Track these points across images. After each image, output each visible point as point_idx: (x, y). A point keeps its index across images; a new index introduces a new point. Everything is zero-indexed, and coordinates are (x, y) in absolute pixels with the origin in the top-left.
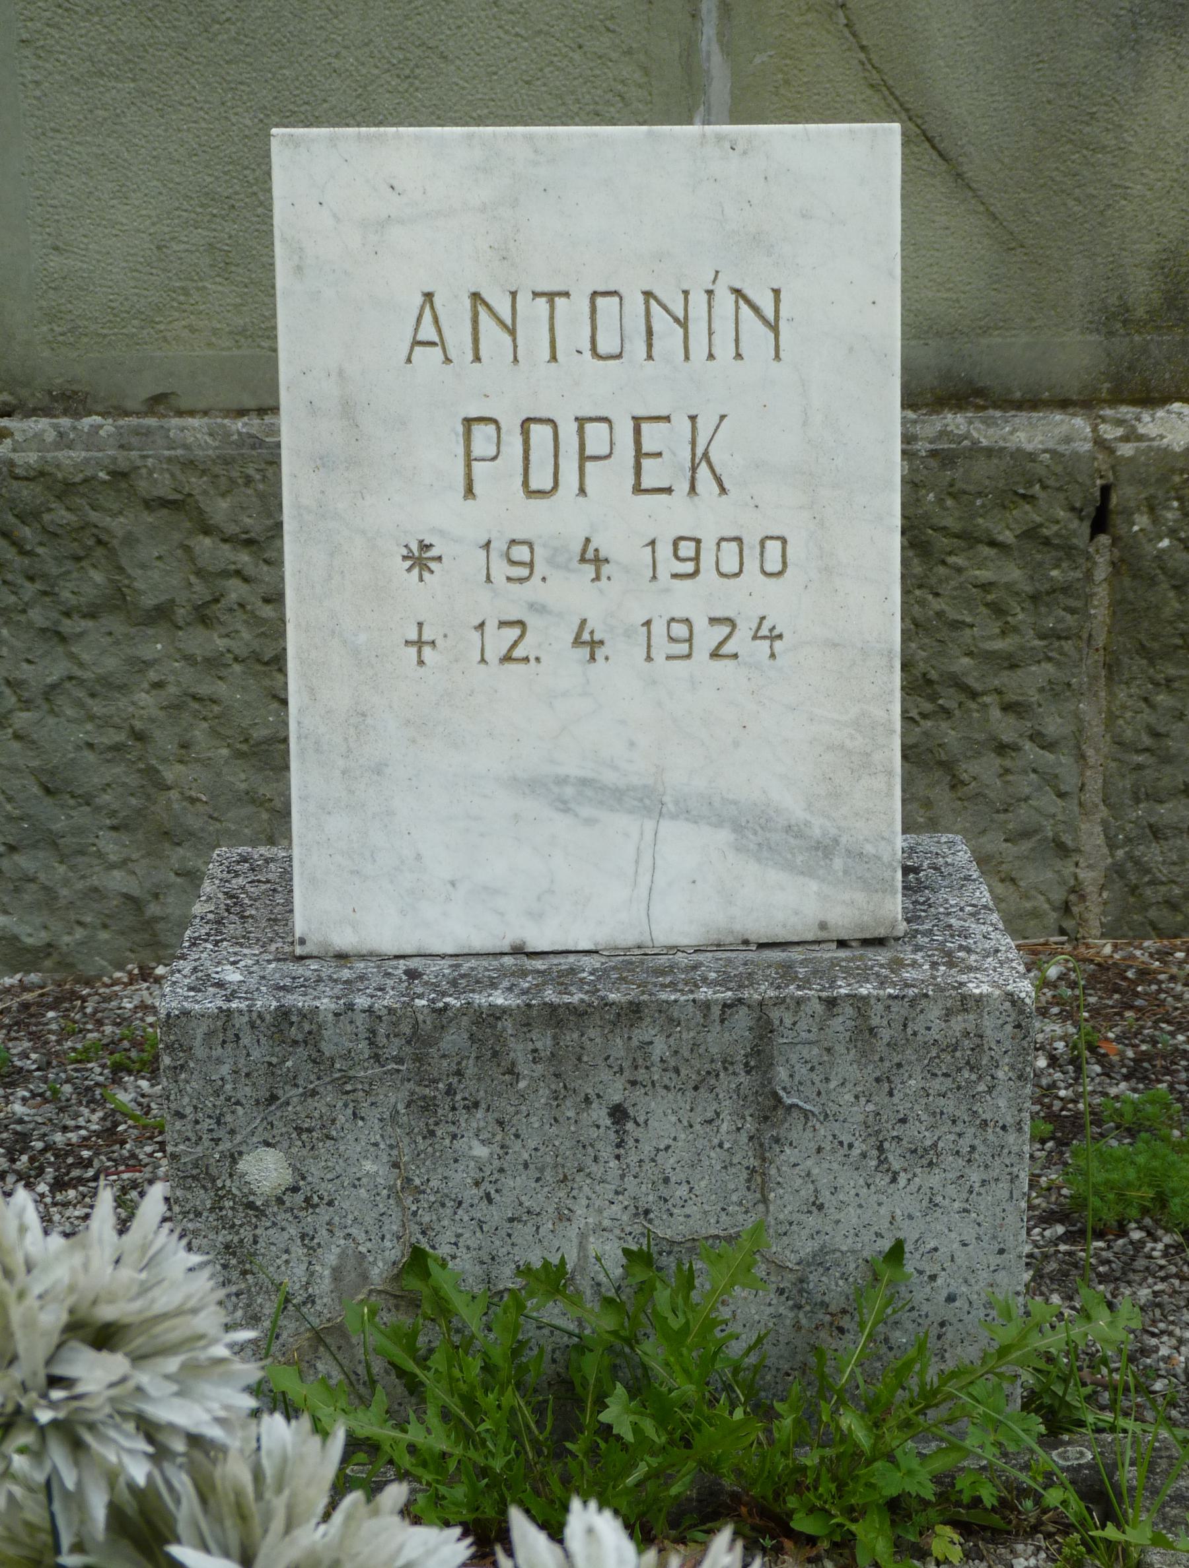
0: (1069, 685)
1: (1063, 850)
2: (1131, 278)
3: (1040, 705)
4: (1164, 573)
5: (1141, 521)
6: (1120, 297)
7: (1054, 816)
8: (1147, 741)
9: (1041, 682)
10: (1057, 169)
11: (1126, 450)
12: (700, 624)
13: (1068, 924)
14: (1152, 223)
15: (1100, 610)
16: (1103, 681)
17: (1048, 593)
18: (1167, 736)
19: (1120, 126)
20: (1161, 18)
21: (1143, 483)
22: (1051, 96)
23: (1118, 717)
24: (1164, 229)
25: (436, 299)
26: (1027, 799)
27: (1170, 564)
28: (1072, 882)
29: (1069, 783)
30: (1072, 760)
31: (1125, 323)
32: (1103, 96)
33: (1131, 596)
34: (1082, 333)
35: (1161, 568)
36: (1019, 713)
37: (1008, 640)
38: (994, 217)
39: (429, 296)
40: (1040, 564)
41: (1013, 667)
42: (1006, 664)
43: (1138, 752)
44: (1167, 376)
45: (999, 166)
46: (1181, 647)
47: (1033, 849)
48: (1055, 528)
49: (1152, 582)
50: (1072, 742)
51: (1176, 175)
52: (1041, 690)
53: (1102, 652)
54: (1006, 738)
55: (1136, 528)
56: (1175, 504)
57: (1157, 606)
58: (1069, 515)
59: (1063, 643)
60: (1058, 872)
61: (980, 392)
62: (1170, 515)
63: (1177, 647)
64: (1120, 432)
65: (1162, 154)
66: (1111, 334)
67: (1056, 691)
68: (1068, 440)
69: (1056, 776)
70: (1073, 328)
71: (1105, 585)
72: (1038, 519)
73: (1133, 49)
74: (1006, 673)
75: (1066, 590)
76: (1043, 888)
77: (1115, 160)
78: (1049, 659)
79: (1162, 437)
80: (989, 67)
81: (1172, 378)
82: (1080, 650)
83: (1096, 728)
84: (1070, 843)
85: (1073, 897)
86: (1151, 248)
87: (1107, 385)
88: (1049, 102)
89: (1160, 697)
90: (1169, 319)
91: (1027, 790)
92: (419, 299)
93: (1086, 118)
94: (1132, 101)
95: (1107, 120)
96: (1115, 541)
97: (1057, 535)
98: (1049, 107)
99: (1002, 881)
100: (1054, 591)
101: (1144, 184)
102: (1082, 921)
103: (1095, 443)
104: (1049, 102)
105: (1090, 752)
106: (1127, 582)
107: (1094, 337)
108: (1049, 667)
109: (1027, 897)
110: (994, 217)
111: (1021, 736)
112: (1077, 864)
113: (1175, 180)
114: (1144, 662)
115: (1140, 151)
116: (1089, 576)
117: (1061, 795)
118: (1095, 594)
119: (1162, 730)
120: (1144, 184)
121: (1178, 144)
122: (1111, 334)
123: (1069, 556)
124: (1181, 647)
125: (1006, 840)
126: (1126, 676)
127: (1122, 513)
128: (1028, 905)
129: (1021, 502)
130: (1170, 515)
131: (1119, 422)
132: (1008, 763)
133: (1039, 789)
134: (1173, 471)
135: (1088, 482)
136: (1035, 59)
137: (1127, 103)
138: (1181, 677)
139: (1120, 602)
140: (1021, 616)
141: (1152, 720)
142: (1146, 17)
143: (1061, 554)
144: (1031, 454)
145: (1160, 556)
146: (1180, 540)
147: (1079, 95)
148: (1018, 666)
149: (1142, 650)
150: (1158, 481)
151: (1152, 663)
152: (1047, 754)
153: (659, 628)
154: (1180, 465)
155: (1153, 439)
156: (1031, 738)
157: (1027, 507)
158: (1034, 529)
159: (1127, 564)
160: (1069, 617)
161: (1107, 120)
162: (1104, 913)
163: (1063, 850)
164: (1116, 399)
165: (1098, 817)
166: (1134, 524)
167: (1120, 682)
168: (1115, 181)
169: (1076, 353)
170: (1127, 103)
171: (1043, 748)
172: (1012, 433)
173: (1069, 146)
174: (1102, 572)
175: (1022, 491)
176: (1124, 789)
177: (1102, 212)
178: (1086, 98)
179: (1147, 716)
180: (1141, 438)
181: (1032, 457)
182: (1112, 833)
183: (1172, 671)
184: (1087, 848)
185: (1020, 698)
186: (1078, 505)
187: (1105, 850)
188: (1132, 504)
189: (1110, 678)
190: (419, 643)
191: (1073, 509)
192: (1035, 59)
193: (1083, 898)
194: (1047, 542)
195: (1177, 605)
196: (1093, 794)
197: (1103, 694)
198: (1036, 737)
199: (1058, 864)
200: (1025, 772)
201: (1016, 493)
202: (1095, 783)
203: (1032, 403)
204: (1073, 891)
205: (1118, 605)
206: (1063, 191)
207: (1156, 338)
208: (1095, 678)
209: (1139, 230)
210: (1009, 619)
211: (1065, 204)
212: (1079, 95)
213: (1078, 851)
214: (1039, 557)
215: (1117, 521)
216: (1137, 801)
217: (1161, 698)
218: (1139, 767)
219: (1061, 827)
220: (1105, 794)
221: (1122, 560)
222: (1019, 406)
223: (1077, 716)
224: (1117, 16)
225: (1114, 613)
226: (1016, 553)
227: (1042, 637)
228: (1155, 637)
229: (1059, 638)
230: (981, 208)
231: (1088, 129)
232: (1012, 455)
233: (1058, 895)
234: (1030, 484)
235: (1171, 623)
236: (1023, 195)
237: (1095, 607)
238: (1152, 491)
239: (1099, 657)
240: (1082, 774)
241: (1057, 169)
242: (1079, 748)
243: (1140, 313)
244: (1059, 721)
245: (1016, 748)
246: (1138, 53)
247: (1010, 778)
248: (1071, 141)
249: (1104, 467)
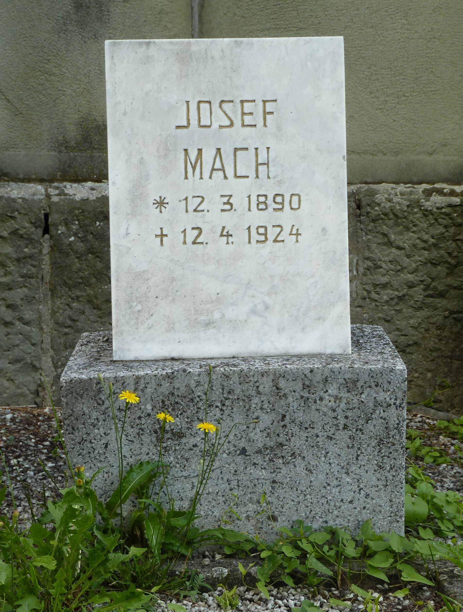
0: (34, 297)
1: (35, 368)
2: (68, 129)
3: (22, 306)
4: (73, 251)
5: (62, 229)
6: (64, 137)
7: (30, 353)
8: (69, 322)
9: (22, 296)
10: (34, 82)
11: (55, 199)
12: (270, 229)
13: (38, 400)
14: (76, 106)
15: (46, 267)
16: (49, 297)
17: (24, 258)
18: (78, 321)
19: (61, 65)
20: (76, 21)
21: (62, 213)
22: (31, 52)
23: (56, 312)
24: (81, 109)
25: (222, 151)
26: (18, 346)
27: (75, 248)
28: (39, 382)
29: (36, 339)
30: (38, 330)
31: (66, 147)
32: (53, 52)
33: (59, 261)
34: (48, 151)
35: (71, 249)
36: (13, 309)
37: (7, 278)
38: (9, 101)
39: (219, 150)
40: (19, 246)
41: (10, 289)
42: (7, 288)
43: (66, 327)
44: (85, 170)
45: (10, 80)
46: (82, 283)
47: (21, 367)
48: (25, 230)
49: (68, 255)
50: (37, 322)
51: (85, 87)
52: (22, 299)
53: (48, 284)
54: (8, 319)
55: (59, 232)
56: (77, 222)
57: (70, 265)
58: (30, 225)
59: (31, 280)
60: (33, 377)
61: (6, 175)
62: (74, 227)
63: (80, 283)
64: (57, 192)
65: (79, 77)
66: (60, 152)
67: (29, 300)
68: (34, 194)
69: (30, 336)
70: (44, 149)
71: (48, 256)
72: (17, 227)
73: (64, 33)
74: (7, 292)
75: (31, 257)
76: (25, 384)
77: (59, 80)
78: (26, 286)
79: (75, 195)
80: (4, 38)
81: (87, 171)
82: (38, 283)
83: (47, 316)
84: (38, 365)
85: (40, 389)
86: (76, 116)
87: (59, 173)
88: (30, 54)
89: (74, 304)
90: (85, 147)
91: (18, 342)
92: (214, 151)
93: (46, 61)
94: (65, 55)
95: (55, 63)
96: (51, 237)
97: (25, 233)
98: (30, 56)
99: (8, 380)
100: (26, 257)
101: (72, 90)
102: (44, 399)
103: (46, 196)
104: (30, 54)
105: (45, 327)
106: (57, 255)
107: (53, 153)
108: (25, 289)
109: (19, 388)
110: (9, 101)
111: (14, 319)
112: (41, 374)
113: (85, 89)
114: (67, 289)
115: (70, 76)
116: (41, 251)
117: (33, 345)
118: (44, 259)
119: (75, 318)
120: (72, 90)
121: (85, 74)
122: (60, 152)
123: (31, 243)
124: (82, 283)
125: (9, 363)
126: (59, 295)
127: (53, 225)
128: (19, 391)
129: (10, 219)
130: (74, 227)
131: (57, 188)
132: (9, 330)
133: (23, 342)
134: (75, 208)
135: (38, 212)
136: (23, 36)
137: (63, 56)
138: (82, 296)
139: (55, 263)
140: (12, 268)
141: (71, 314)
142: (69, 20)
143: (28, 242)
144: (13, 199)
145: (70, 244)
146: (79, 237)
147: (43, 51)
148: (12, 289)
149: (65, 284)
150: (68, 212)
151: (70, 290)
152: (26, 327)
153: (253, 231)
154: (77, 206)
155: (71, 195)
156: (19, 319)
157: (13, 221)
158: (16, 230)
159: (56, 247)
160: (33, 269)
161: (55, 63)
162: (54, 396)
163: (35, 368)
164: (64, 178)
165: (49, 354)
166: (58, 230)
167: (57, 297)
168: (59, 88)
169: (45, 158)
170: (63, 56)
171: (24, 324)
172: (11, 191)
173: (39, 73)
174: (46, 250)
175: (10, 215)
176: (60, 343)
177: (54, 101)
178: (45, 53)
179: (68, 312)
180: (66, 195)
181: (14, 200)
182: (55, 362)
183: (79, 293)
184: (44, 368)
185: (13, 303)
186: (33, 221)
187: (53, 369)
188: (58, 222)
189: (52, 296)
190: (162, 235)
191: (32, 223)
192: (23, 36)
193: (44, 389)
194: (21, 236)
195: (78, 265)
196: (47, 344)
197: (50, 302)
198: (20, 319)
199: (34, 374)
200: (16, 334)
201: (7, 215)
202: (47, 340)
203: (28, 180)
204: (40, 386)
205: (54, 264)
206: (38, 91)
207: (79, 154)
208: (47, 295)
209: (71, 109)
210: (7, 269)
211: (38, 97)
212: (43, 51)
213: (41, 368)
214: (19, 243)
215: (51, 228)
216: (67, 348)
217: (75, 305)
218: (66, 334)
219: (33, 358)
220: (52, 345)
221: (55, 246)
222: (23, 181)
223: (38, 310)
224: (57, 20)
225: (52, 268)
226: (9, 241)
227: (22, 277)
228: (70, 279)
229: (29, 278)
230: (3, 97)
231: (47, 66)
232: (6, 199)
233: (33, 387)
234: (13, 212)
235: (76, 272)
236: (21, 92)
237: (44, 265)
238: (66, 216)
239: (48, 286)
240: (42, 336)
241: (34, 82)
242: (40, 325)
243: (73, 143)
244: (31, 313)
245: (12, 324)
246: (67, 35)
247: (10, 336)
248: (40, 71)
249: (45, 206)
